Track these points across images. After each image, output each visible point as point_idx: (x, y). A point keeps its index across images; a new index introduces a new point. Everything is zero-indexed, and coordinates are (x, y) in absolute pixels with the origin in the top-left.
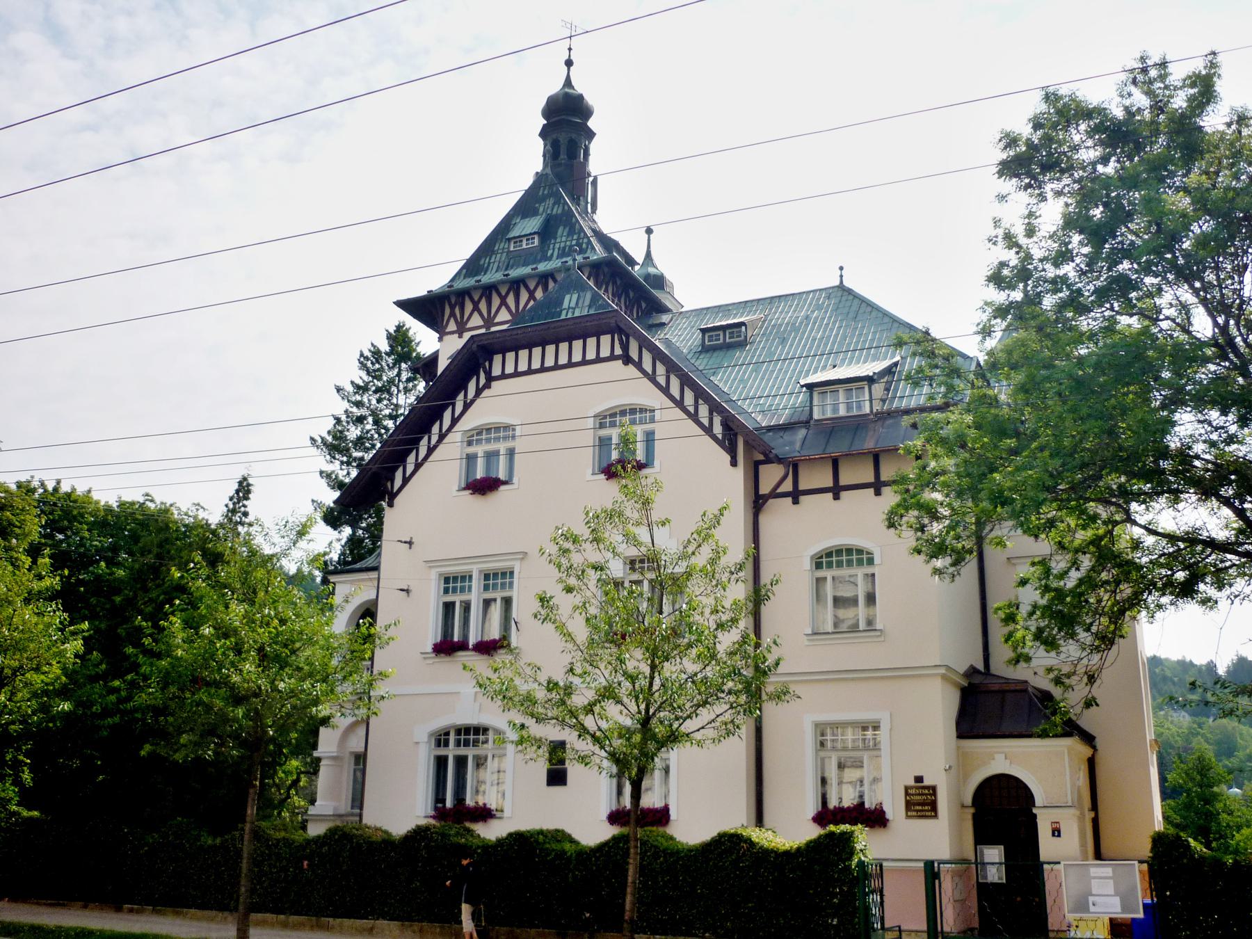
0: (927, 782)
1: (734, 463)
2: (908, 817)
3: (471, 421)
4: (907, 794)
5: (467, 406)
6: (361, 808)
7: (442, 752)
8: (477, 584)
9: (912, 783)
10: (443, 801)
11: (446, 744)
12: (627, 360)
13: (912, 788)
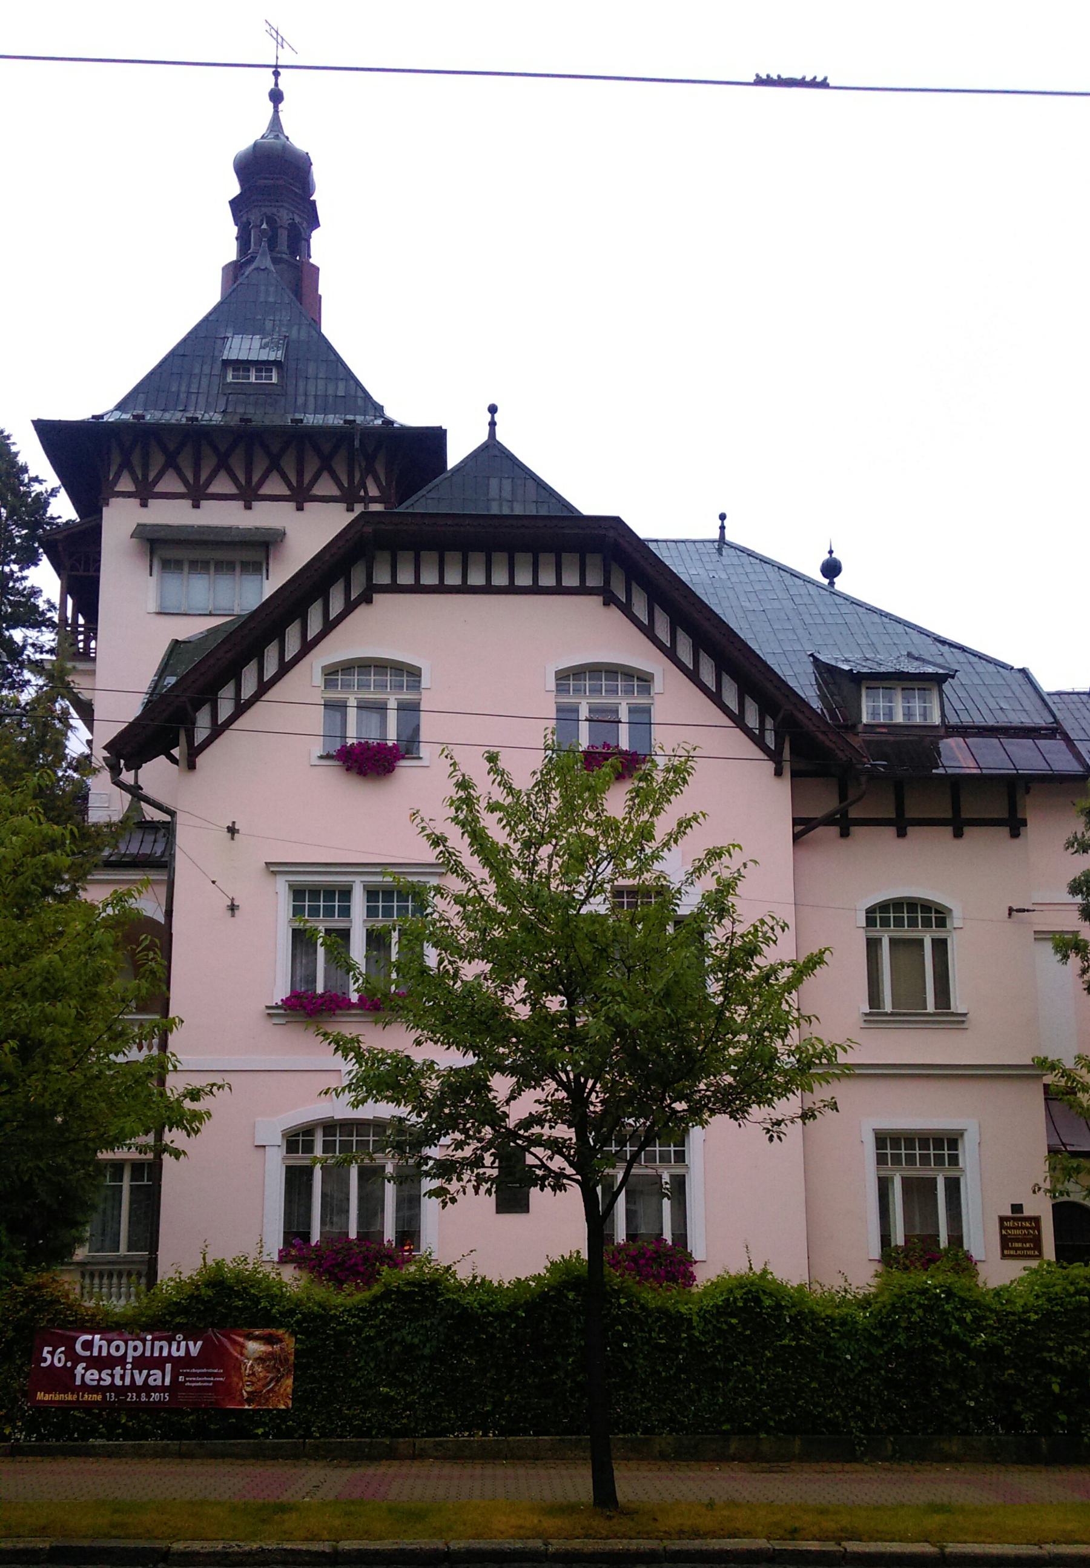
0: (1027, 1213)
1: (778, 773)
2: (1004, 1256)
3: (338, 648)
4: (1002, 1227)
5: (329, 626)
6: (153, 1245)
7: (300, 1159)
8: (358, 903)
9: (1008, 1213)
10: (306, 1236)
11: (309, 1148)
12: (610, 599)
13: (1007, 1219)
